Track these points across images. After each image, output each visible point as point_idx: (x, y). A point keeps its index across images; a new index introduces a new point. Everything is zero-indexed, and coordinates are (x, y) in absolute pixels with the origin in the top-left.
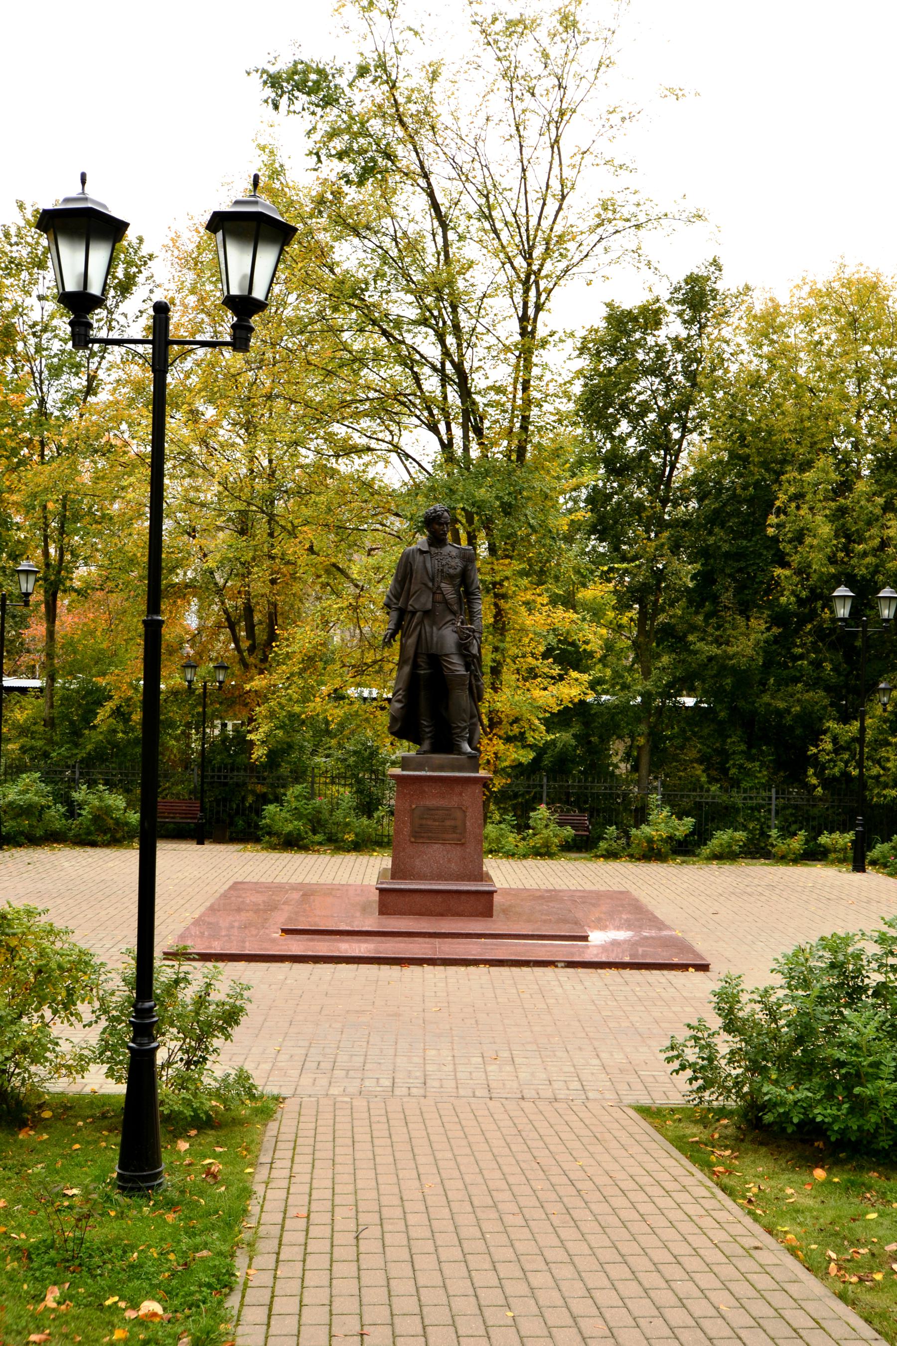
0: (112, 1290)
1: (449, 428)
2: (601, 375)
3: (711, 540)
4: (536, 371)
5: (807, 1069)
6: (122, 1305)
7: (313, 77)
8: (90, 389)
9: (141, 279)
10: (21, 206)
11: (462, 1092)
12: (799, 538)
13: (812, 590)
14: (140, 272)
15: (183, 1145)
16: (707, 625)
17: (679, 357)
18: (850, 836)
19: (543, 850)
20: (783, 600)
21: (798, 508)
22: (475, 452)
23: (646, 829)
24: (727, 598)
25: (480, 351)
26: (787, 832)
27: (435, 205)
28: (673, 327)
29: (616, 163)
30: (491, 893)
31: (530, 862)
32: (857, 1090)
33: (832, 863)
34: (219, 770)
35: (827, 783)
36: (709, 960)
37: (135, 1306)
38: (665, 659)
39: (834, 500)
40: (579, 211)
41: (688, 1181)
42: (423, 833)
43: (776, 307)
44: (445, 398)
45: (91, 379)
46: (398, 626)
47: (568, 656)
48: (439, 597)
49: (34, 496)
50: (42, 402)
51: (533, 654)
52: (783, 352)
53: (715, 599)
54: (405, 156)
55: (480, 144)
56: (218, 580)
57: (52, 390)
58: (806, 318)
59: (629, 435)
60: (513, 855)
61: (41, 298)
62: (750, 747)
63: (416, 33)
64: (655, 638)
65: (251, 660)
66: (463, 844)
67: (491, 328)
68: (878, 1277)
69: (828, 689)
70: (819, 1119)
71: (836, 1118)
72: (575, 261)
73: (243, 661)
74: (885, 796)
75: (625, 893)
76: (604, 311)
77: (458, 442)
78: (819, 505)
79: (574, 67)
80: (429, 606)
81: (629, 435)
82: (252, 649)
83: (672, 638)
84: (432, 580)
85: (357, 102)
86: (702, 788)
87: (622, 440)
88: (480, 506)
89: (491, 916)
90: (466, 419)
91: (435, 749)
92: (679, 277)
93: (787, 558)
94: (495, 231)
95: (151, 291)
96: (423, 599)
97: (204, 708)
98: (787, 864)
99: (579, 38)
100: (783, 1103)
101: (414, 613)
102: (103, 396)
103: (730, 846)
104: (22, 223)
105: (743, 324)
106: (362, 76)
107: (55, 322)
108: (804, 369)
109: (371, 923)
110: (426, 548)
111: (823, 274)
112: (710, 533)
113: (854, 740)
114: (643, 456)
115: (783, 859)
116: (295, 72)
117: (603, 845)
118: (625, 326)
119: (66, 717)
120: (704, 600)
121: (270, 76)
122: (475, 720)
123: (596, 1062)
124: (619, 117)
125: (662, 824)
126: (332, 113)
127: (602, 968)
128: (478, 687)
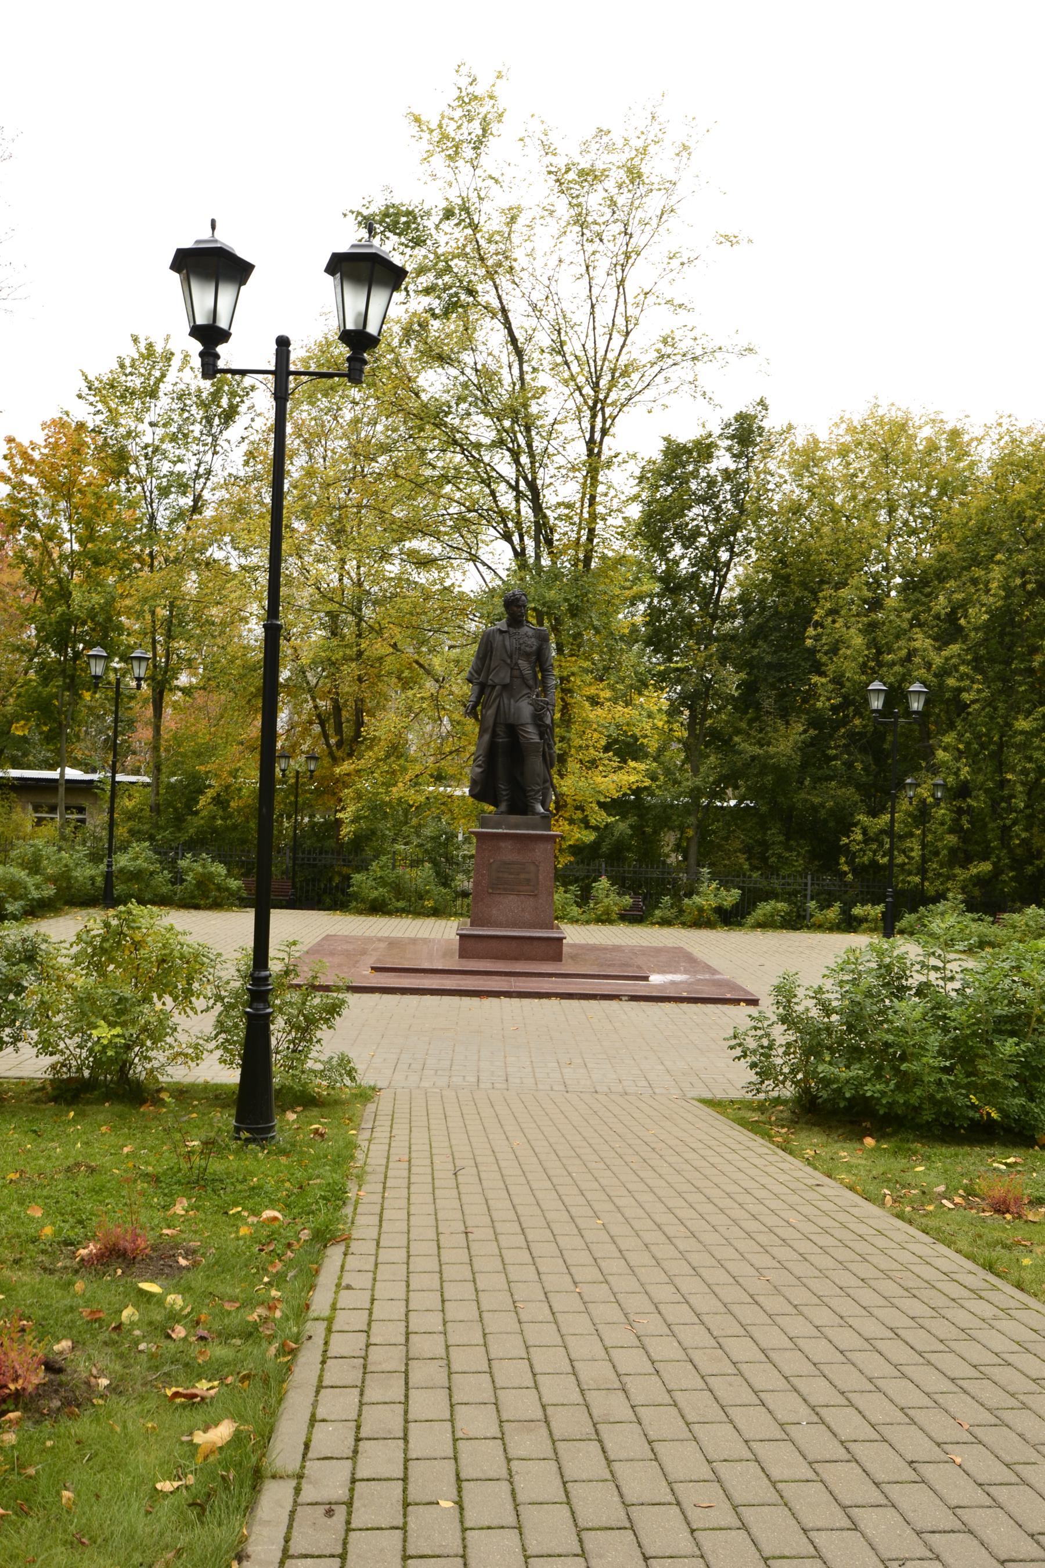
0: (235, 1204)
1: (521, 539)
2: (657, 501)
4: (601, 489)
5: (854, 1054)
6: (246, 1214)
7: (403, 219)
8: (196, 509)
9: (243, 409)
10: (136, 340)
11: (540, 1087)
12: (834, 650)
13: (845, 697)
14: (242, 401)
15: (291, 1116)
16: (751, 728)
17: (728, 487)
18: (880, 908)
19: (604, 917)
20: (819, 705)
21: (834, 622)
23: (696, 898)
24: (768, 704)
25: (551, 470)
27: (514, 340)
28: (723, 461)
29: (676, 302)
31: (592, 927)
32: (904, 1067)
34: (309, 853)
35: (854, 871)
36: (758, 996)
37: (255, 1213)
38: (712, 758)
39: (867, 616)
40: (641, 347)
41: (751, 1144)
43: (816, 442)
44: (518, 511)
45: (197, 498)
46: (481, 693)
47: (625, 748)
48: (516, 673)
49: (144, 600)
50: (152, 517)
51: (594, 747)
52: (822, 480)
53: (758, 707)
54: (487, 295)
55: (553, 283)
56: (310, 678)
57: (161, 508)
58: (843, 452)
59: (683, 557)
60: (577, 921)
61: (152, 424)
62: (788, 839)
63: (497, 181)
64: (703, 739)
65: (339, 754)
67: (561, 449)
68: (931, 1208)
69: (859, 787)
70: (869, 1094)
71: (883, 1094)
72: (638, 389)
73: (331, 754)
74: (909, 883)
75: (680, 949)
76: (662, 445)
77: (530, 551)
78: (853, 619)
79: (639, 214)
80: (507, 681)
81: (683, 557)
82: (340, 744)
83: (720, 740)
84: (511, 657)
85: (443, 244)
86: (744, 875)
87: (677, 563)
88: (550, 605)
89: (560, 960)
90: (538, 531)
91: (513, 810)
92: (730, 414)
93: (823, 668)
94: (566, 363)
95: (253, 420)
96: (502, 675)
97: (296, 797)
98: (824, 932)
99: (643, 189)
100: (836, 1080)
101: (493, 687)
102: (209, 513)
103: (772, 916)
104: (136, 356)
105: (786, 457)
106: (448, 218)
107: (164, 446)
108: (841, 497)
109: (455, 963)
110: (505, 628)
112: (754, 646)
113: (882, 832)
114: (695, 576)
115: (819, 927)
116: (387, 215)
119: (169, 804)
120: (748, 707)
121: (365, 218)
122: (548, 784)
123: (661, 1067)
124: (679, 261)
125: (710, 895)
126: (420, 252)
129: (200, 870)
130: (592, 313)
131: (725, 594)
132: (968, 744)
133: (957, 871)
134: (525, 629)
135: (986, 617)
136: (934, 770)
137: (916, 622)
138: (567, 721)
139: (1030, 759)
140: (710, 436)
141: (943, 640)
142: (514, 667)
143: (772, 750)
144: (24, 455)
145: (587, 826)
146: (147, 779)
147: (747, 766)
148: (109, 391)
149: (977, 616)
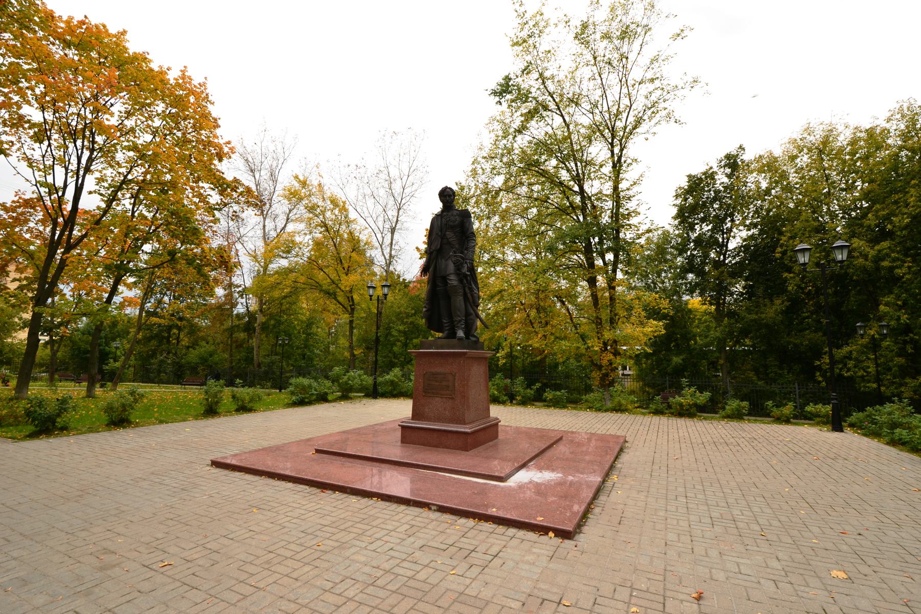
31: (609, 415)
33: (818, 424)
66: (452, 398)
76: (686, 179)
98: (781, 423)
109: (396, 452)
115: (779, 420)
133: (908, 380)
140: (711, 168)
143: (763, 316)
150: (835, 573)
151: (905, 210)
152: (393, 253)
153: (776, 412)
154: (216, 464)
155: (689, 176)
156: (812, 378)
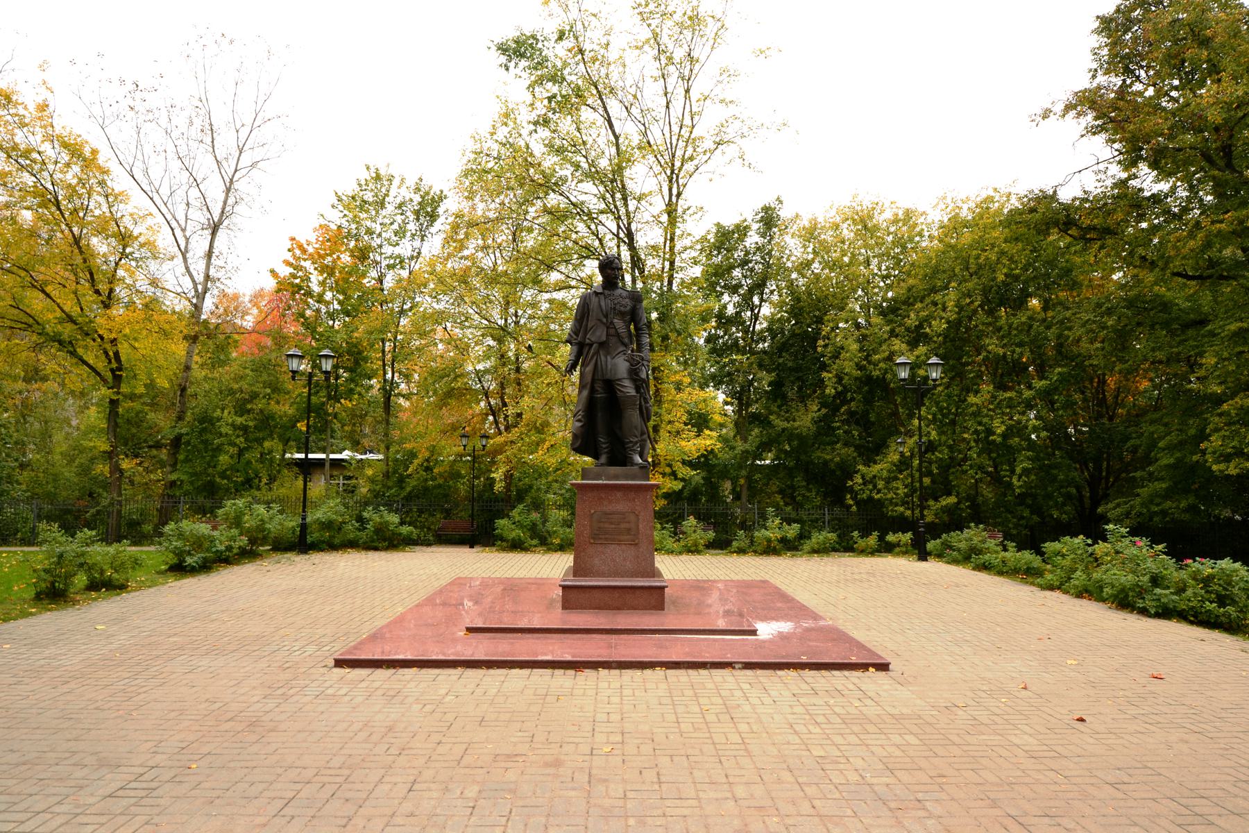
3: (781, 360)
10: (368, 168)
12: (836, 356)
22: (639, 285)
26: (865, 534)
28: (753, 239)
30: (662, 588)
31: (684, 557)
33: (898, 554)
35: (858, 503)
36: (887, 657)
42: (601, 536)
46: (579, 354)
48: (612, 331)
53: (784, 397)
64: (744, 422)
80: (604, 338)
89: (663, 609)
96: (598, 333)
101: (591, 345)
109: (558, 617)
111: (844, 200)
117: (735, 544)
118: (726, 238)
122: (645, 436)
125: (773, 530)
127: (780, 669)
128: (647, 409)
129: (378, 520)
130: (667, 107)
131: (758, 327)
132: (934, 415)
134: (619, 291)
135: (945, 326)
136: (910, 434)
137: (893, 333)
138: (659, 403)
139: (980, 424)
141: (913, 344)
142: (610, 326)
143: (797, 424)
144: (301, 247)
145: (676, 479)
146: (381, 457)
147: (779, 435)
148: (356, 204)
149: (939, 326)
150: (1069, 662)
151: (944, 315)
152: (212, 272)
153: (861, 543)
154: (339, 663)
155: (718, 225)
156: (840, 501)
